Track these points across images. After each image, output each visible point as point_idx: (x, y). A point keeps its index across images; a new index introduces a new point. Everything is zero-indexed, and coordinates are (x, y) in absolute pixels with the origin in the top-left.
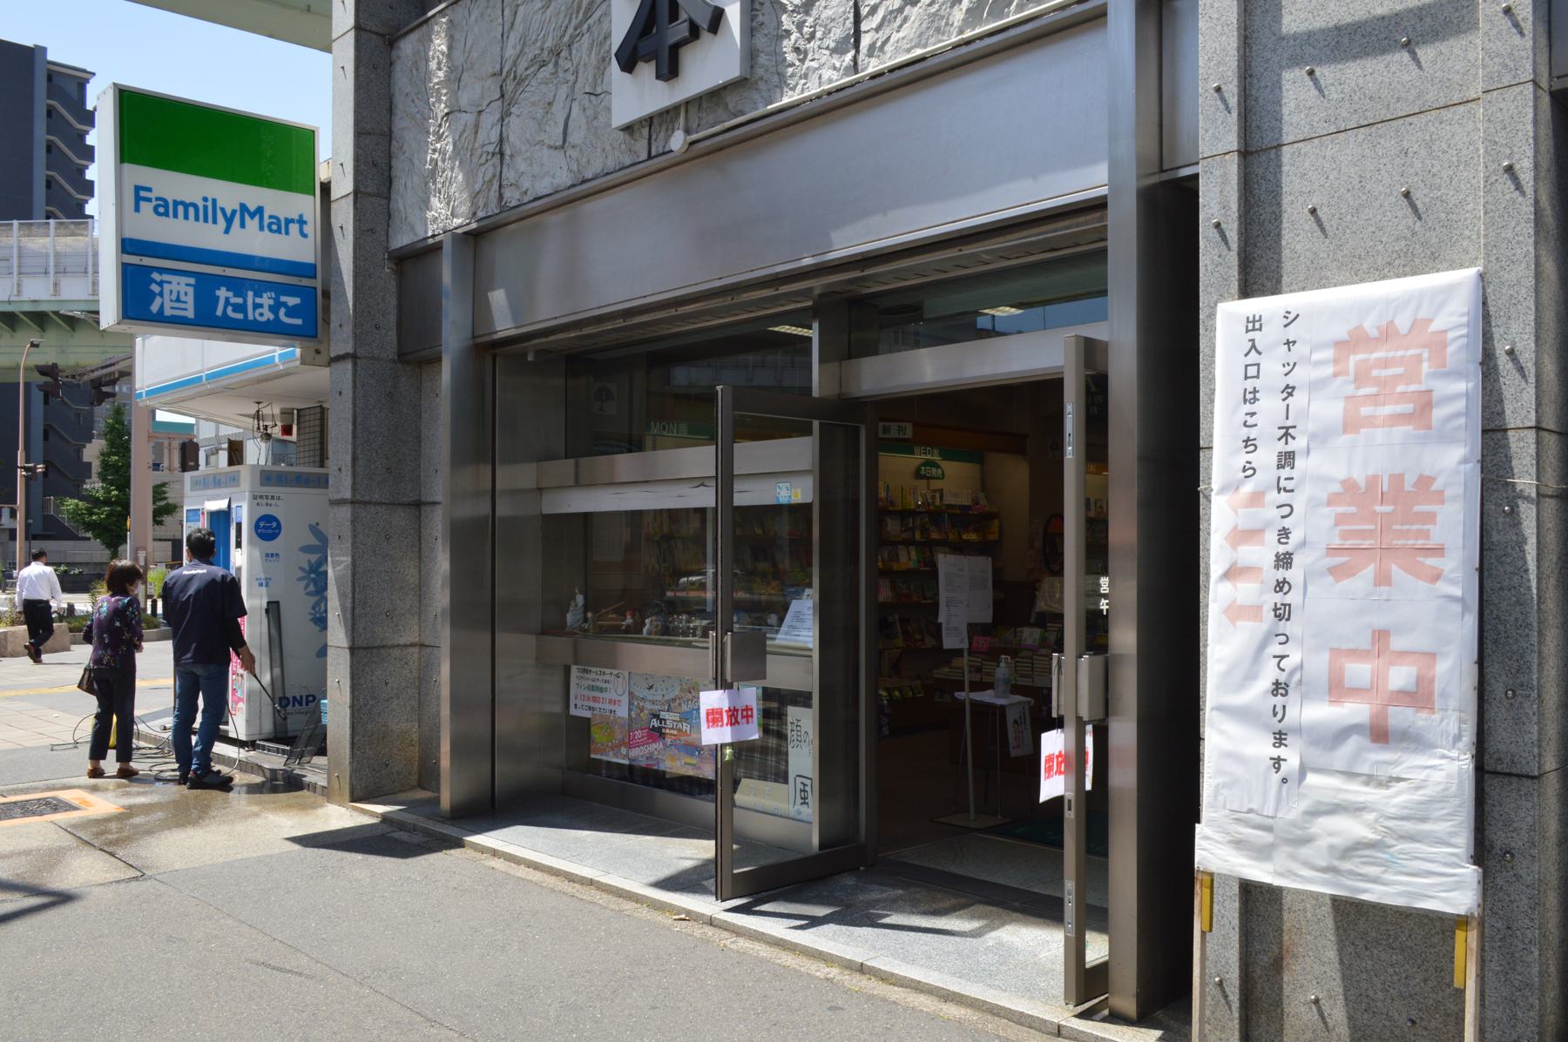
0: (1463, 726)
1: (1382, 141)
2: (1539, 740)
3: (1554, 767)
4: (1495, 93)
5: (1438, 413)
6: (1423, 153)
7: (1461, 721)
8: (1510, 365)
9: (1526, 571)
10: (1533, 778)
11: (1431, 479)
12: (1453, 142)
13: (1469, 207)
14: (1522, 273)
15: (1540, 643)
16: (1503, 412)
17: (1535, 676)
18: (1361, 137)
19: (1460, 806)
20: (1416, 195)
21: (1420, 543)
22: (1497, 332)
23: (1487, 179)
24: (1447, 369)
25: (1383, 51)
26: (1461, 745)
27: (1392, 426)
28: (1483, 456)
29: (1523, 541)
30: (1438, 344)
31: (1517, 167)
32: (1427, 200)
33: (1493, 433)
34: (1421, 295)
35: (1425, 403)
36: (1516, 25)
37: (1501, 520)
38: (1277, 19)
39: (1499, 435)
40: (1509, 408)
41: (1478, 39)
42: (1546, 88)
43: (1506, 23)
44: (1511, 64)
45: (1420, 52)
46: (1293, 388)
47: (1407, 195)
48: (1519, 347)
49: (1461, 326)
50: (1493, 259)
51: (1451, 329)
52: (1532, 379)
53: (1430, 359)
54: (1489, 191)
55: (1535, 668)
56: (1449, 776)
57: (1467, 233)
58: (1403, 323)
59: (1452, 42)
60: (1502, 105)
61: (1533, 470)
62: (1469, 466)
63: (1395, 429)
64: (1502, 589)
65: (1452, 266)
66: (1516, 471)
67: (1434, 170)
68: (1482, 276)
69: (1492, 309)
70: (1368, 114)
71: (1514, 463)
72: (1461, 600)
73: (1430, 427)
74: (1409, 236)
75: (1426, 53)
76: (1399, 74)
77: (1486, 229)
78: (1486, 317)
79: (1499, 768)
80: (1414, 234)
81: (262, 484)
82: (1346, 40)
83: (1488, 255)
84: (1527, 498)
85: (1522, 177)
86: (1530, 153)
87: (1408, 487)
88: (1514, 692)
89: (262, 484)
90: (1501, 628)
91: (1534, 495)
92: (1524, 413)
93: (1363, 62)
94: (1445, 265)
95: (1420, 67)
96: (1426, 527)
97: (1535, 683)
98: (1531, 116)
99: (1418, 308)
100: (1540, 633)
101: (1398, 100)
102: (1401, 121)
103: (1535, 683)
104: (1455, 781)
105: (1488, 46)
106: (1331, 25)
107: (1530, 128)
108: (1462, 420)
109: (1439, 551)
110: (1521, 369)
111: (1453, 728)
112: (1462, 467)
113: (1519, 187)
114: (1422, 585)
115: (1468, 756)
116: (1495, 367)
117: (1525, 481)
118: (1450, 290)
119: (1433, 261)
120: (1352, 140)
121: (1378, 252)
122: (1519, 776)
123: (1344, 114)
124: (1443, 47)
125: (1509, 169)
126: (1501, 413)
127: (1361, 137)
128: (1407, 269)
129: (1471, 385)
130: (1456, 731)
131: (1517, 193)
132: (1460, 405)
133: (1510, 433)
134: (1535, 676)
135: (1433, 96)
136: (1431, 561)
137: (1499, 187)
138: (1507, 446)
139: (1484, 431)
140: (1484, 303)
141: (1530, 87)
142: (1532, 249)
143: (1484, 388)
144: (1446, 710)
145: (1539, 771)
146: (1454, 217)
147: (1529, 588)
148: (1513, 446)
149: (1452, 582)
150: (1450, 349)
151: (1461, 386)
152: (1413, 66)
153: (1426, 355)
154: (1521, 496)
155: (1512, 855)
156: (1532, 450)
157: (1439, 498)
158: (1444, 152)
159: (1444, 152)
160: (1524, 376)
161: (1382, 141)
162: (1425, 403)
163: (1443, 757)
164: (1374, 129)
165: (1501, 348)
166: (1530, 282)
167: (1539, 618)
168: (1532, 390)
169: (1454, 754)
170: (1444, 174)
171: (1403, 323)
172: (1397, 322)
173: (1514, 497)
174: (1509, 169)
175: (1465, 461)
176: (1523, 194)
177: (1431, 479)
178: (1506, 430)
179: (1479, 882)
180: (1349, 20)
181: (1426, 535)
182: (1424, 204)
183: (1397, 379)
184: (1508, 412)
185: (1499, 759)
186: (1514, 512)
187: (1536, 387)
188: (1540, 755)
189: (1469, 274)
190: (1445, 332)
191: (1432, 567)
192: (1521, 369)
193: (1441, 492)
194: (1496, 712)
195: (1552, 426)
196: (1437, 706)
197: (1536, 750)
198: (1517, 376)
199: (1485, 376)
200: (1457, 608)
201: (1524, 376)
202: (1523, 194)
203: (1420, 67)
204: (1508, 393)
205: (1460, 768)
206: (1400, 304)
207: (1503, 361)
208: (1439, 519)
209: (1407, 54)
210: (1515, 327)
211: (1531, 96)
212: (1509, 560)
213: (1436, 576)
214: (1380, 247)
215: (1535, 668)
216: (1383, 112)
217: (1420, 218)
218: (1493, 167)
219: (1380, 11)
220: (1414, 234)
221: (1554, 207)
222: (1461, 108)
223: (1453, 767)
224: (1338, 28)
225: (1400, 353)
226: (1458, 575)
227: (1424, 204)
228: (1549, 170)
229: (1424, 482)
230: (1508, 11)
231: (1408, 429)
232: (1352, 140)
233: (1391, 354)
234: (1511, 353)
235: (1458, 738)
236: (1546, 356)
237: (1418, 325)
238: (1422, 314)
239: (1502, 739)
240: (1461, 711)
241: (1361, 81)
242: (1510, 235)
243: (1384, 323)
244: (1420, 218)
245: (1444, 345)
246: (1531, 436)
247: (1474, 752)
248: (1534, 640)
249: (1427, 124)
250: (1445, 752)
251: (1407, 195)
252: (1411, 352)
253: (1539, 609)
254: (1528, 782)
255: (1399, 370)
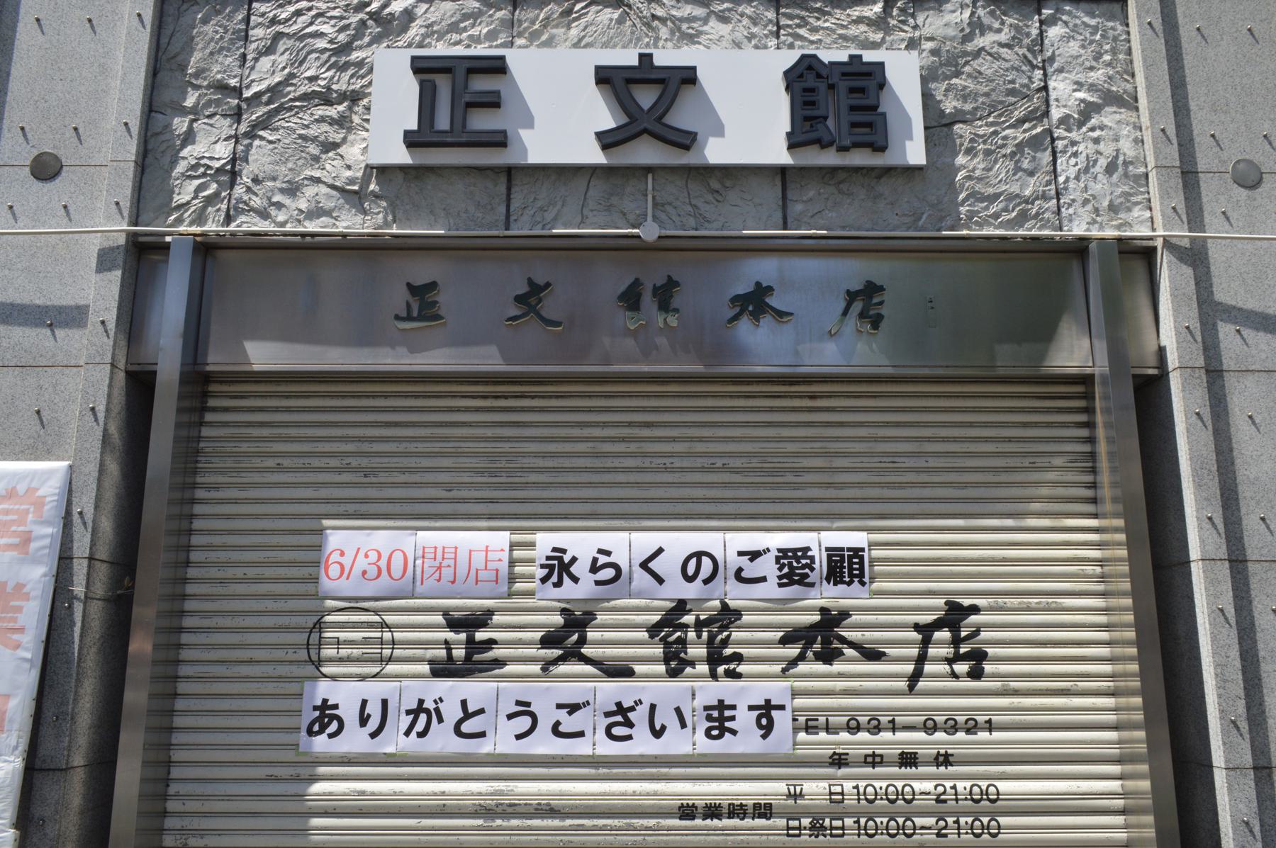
0: (20, 740)
1: (28, 378)
2: (69, 746)
3: (82, 763)
4: (91, 365)
5: (34, 546)
6: (51, 389)
7: (19, 737)
8: (79, 521)
9: (73, 643)
10: (62, 770)
11: (24, 586)
12: (68, 387)
13: (71, 426)
14: (92, 469)
15: (76, 686)
16: (72, 547)
17: (70, 707)
18: (16, 373)
19: (10, 792)
20: (43, 413)
21: (11, 625)
22: (75, 500)
23: (81, 412)
24: (43, 519)
25: (37, 326)
26: (17, 752)
27: (4, 551)
28: (58, 573)
29: (73, 624)
30: (39, 503)
31: (97, 409)
32: (49, 418)
33: (65, 560)
34: (35, 473)
35: (27, 539)
36: (106, 331)
37: (63, 612)
38: (123, 274)
39: (68, 561)
40: (75, 545)
41: (87, 332)
42: (123, 368)
43: (101, 328)
44: (101, 352)
45: (57, 332)
46: (955, 615)
47: (38, 412)
48: (85, 510)
49: (55, 494)
50: (78, 458)
51: (49, 496)
52: (90, 530)
53: (34, 512)
54: (81, 420)
55: (71, 702)
56: (7, 773)
57: (68, 440)
58: (21, 488)
59: (75, 331)
60: (94, 373)
61: (84, 583)
62: (47, 578)
63: (6, 553)
64: (58, 654)
65: (58, 459)
66: (75, 583)
67: (55, 401)
68: (71, 467)
69: (74, 487)
70: (22, 360)
71: (75, 578)
72: (31, 661)
73: (27, 553)
74: (36, 436)
75: (60, 333)
76: (43, 341)
77: (77, 440)
78: (70, 491)
79: (43, 767)
80: (39, 436)
81: (882, 64)
82: (16, 313)
83: (75, 455)
84: (79, 599)
85: (99, 414)
86: (105, 403)
87: (9, 589)
88: (57, 717)
89: (882, 64)
90: (55, 678)
91: (83, 597)
92: (83, 549)
93: (24, 329)
94: (54, 457)
95: (56, 341)
96: (15, 615)
97: (70, 710)
98: (107, 382)
99: (32, 480)
100: (78, 680)
101: (41, 356)
102: (41, 369)
103: (70, 710)
104: (10, 776)
105: (91, 338)
106: (8, 301)
107: (106, 389)
108: (47, 551)
109: (21, 630)
110: (85, 524)
111: (13, 742)
112: (43, 579)
113: (96, 420)
114: (8, 652)
115: (20, 759)
116: (71, 521)
117: (79, 589)
118: (51, 472)
119: (47, 454)
120: (11, 373)
121: (17, 443)
122: (54, 770)
123: (9, 357)
124: (70, 332)
125: (93, 409)
126: (71, 548)
127: (16, 373)
128: (32, 456)
129: (55, 530)
130: (15, 744)
131: (95, 423)
132: (47, 541)
133: (75, 560)
134: (70, 707)
135: (60, 359)
136: (16, 637)
137: (86, 418)
138: (71, 568)
139: (60, 558)
140: (70, 483)
141: (109, 366)
142: (99, 456)
143: (63, 532)
144: (11, 731)
145: (67, 764)
146: (63, 431)
147: (73, 653)
148: (75, 567)
149: (26, 649)
150: (47, 508)
151: (49, 530)
152: (51, 338)
153: (32, 510)
154: (76, 598)
155: (44, 821)
156: (85, 571)
157: (27, 597)
158: (62, 392)
159: (62, 392)
160: (86, 528)
161: (28, 378)
162: (27, 539)
163: (6, 761)
164: (25, 369)
165: (76, 510)
166: (96, 474)
167: (78, 671)
168: (89, 536)
169: (12, 758)
170: (61, 404)
171: (21, 488)
172: (18, 487)
173: (72, 598)
174: (93, 409)
175: (45, 575)
176: (98, 424)
177: (24, 586)
178: (72, 558)
179: (15, 840)
180: (19, 301)
181: (15, 620)
182: (47, 419)
183: (13, 522)
184: (75, 548)
185: (44, 760)
186: (70, 607)
187: (92, 535)
188: (69, 756)
189: (65, 464)
190: (45, 497)
191: (17, 640)
192: (85, 524)
193: (28, 594)
194: (46, 731)
195: (104, 557)
196: (6, 728)
197: (66, 753)
198: (83, 527)
199: (65, 526)
200: (27, 666)
201: (86, 528)
202: (98, 424)
203: (56, 341)
204: (76, 536)
205: (14, 767)
206: (23, 476)
207: (76, 518)
208: (24, 610)
209: (49, 331)
210: (85, 499)
211: (109, 372)
212: (64, 636)
213: (18, 646)
214: (18, 441)
215: (71, 702)
216: (32, 361)
217: (44, 428)
218: (85, 406)
219: (38, 302)
220: (39, 436)
221: (122, 434)
222: (75, 369)
223: (9, 767)
224: (12, 305)
225: (17, 507)
226: (31, 645)
227: (47, 419)
228: (119, 413)
229: (19, 587)
230: (103, 322)
231: (14, 553)
232: (11, 373)
233: (11, 507)
234: (81, 513)
235: (16, 748)
236: (103, 517)
237: (31, 490)
238: (34, 485)
239: (46, 749)
240: (20, 731)
241: (21, 339)
242: (89, 446)
243: (11, 487)
244: (44, 428)
245: (43, 504)
246: (85, 563)
247: (25, 757)
248: (73, 685)
249: (55, 374)
250: (7, 758)
251: (38, 412)
252: (23, 507)
253: (79, 665)
254: (58, 773)
255: (15, 517)
